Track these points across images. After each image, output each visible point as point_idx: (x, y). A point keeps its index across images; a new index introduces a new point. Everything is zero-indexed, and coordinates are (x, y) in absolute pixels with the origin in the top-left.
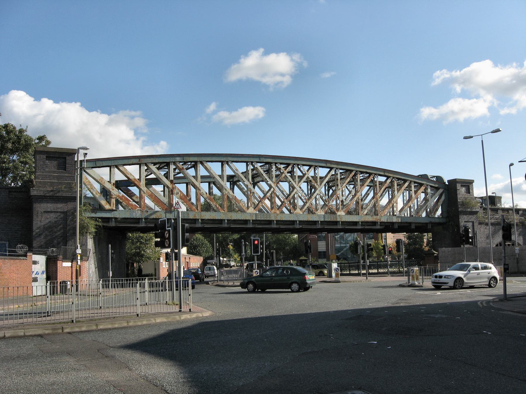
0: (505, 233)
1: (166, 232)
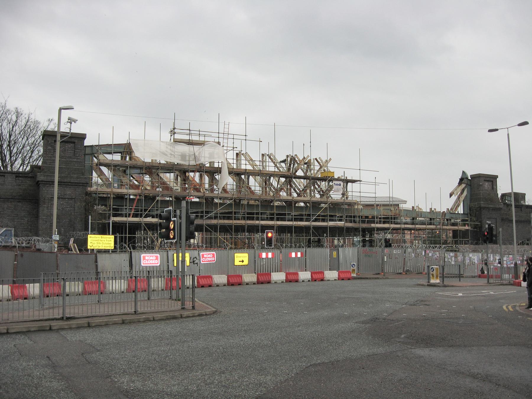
1: (172, 223)
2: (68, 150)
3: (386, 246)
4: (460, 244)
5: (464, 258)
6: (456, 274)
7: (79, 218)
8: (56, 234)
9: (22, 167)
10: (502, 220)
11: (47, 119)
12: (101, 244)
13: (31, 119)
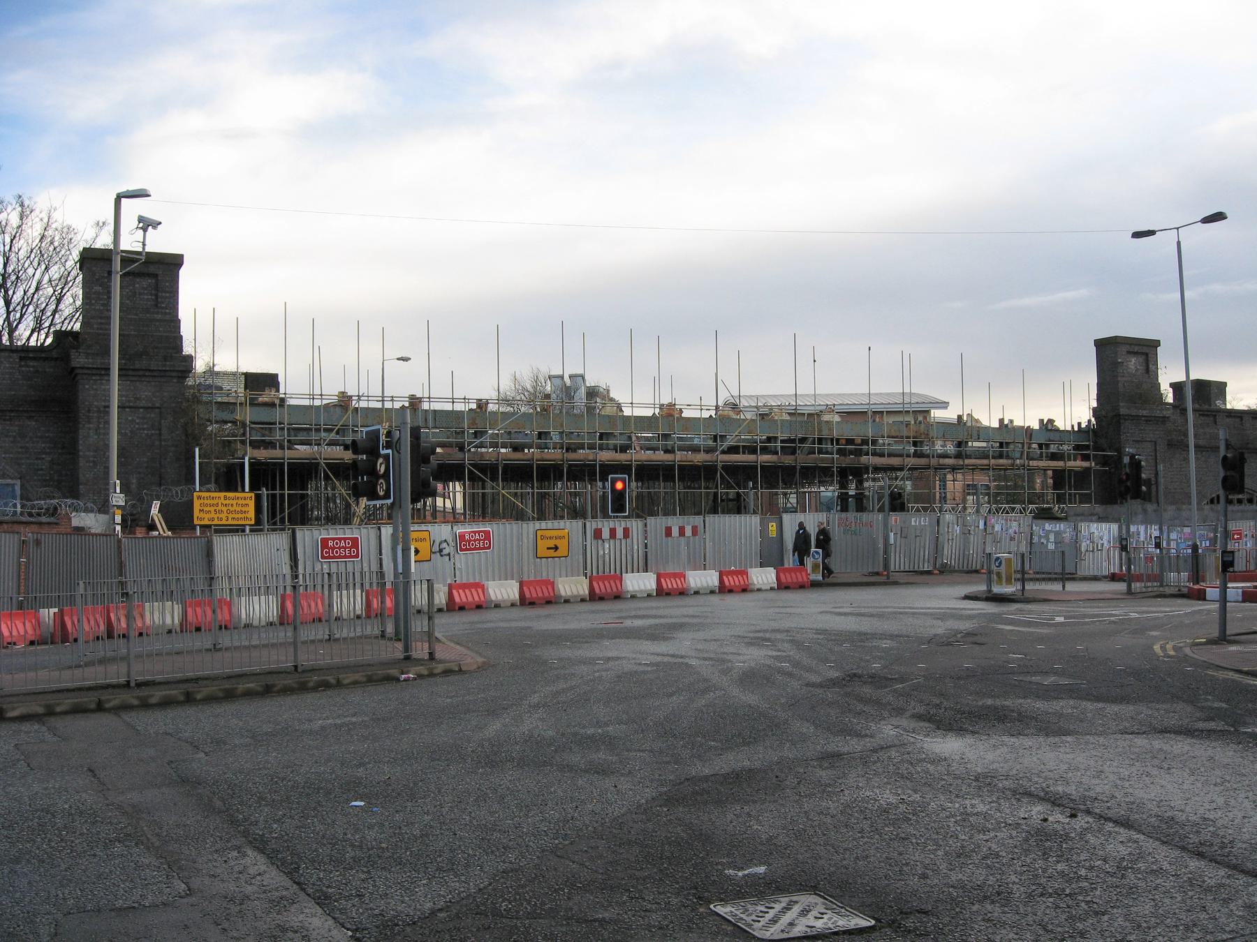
0: (1228, 473)
1: (381, 460)
2: (140, 294)
3: (893, 509)
4: (1071, 503)
5: (1077, 534)
6: (1056, 574)
7: (171, 454)
8: (118, 491)
9: (36, 334)
10: (1168, 445)
11: (92, 222)
12: (226, 514)
13: (56, 221)
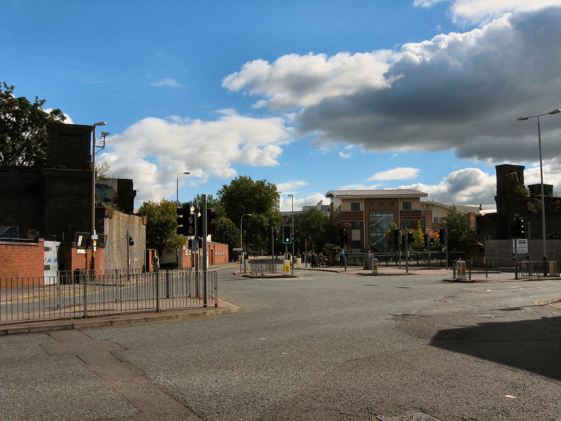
1: (190, 218)
